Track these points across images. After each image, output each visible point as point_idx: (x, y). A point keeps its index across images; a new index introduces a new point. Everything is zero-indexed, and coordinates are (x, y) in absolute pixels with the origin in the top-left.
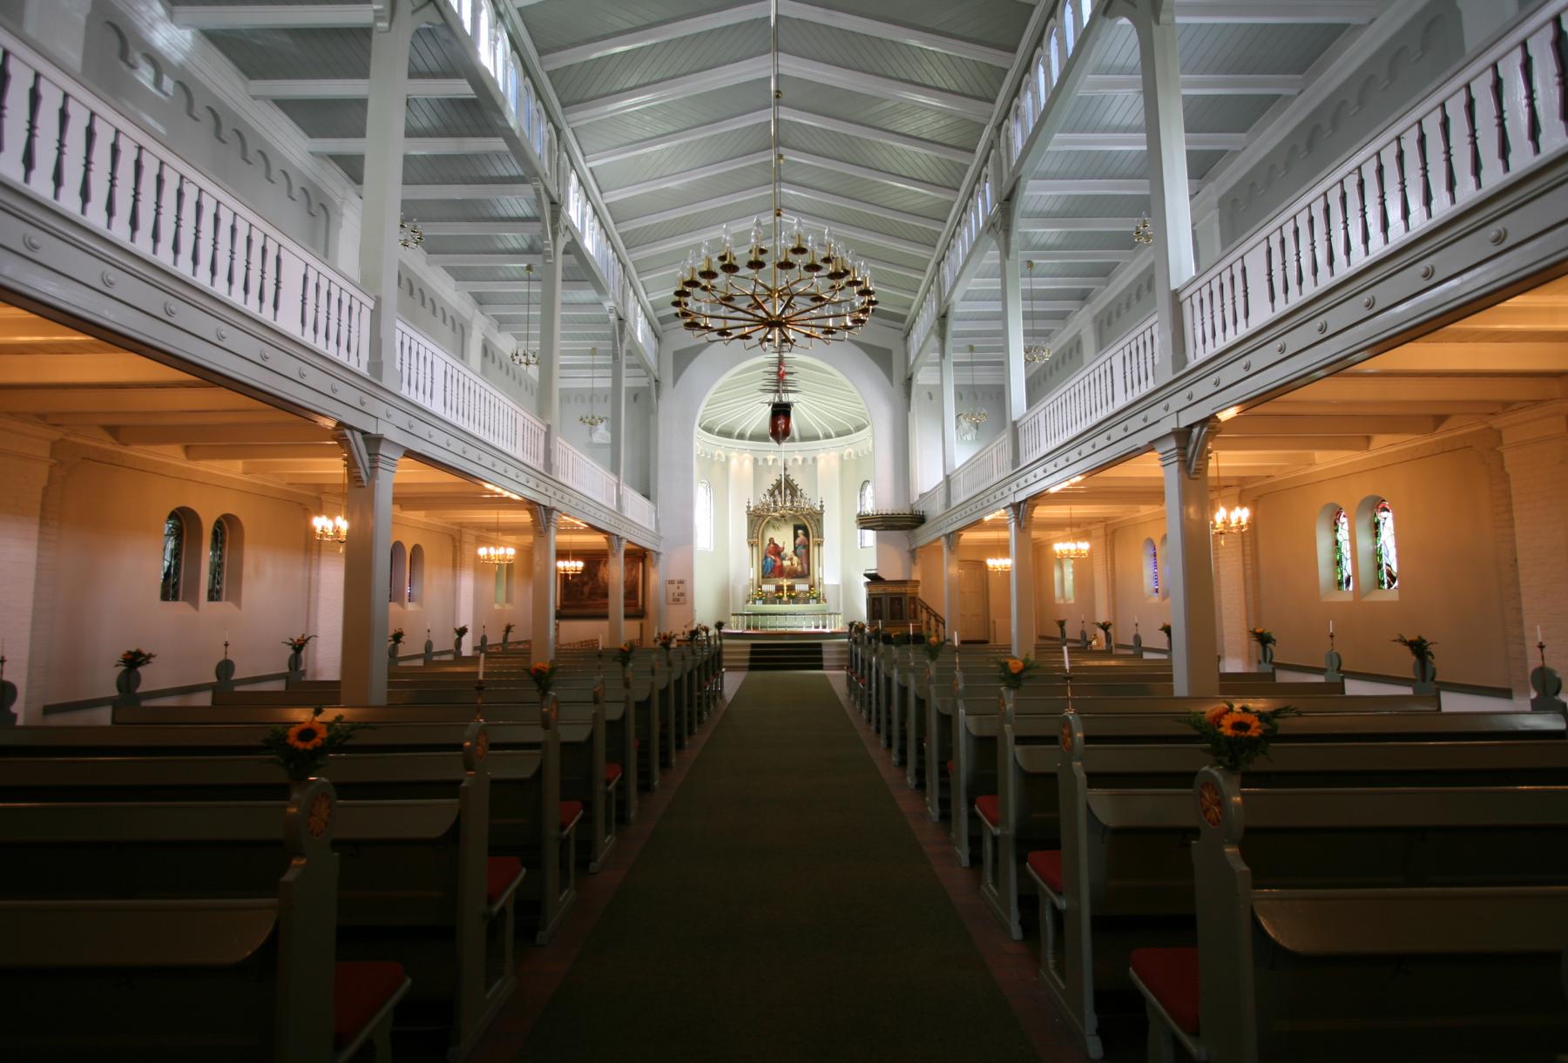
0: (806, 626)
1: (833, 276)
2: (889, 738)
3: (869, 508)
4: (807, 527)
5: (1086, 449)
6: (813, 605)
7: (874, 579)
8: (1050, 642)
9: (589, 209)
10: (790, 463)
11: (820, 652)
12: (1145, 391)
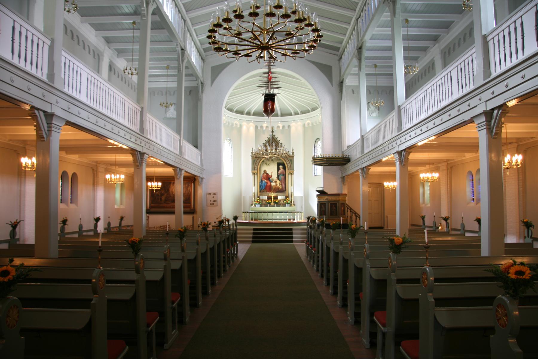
0: (283, 218)
1: (297, 21)
2: (328, 280)
3: (319, 153)
4: (285, 164)
5: (438, 121)
6: (287, 208)
7: (322, 193)
8: (417, 227)
9: (193, 43)
10: (275, 129)
11: (292, 233)
12: (469, 90)
